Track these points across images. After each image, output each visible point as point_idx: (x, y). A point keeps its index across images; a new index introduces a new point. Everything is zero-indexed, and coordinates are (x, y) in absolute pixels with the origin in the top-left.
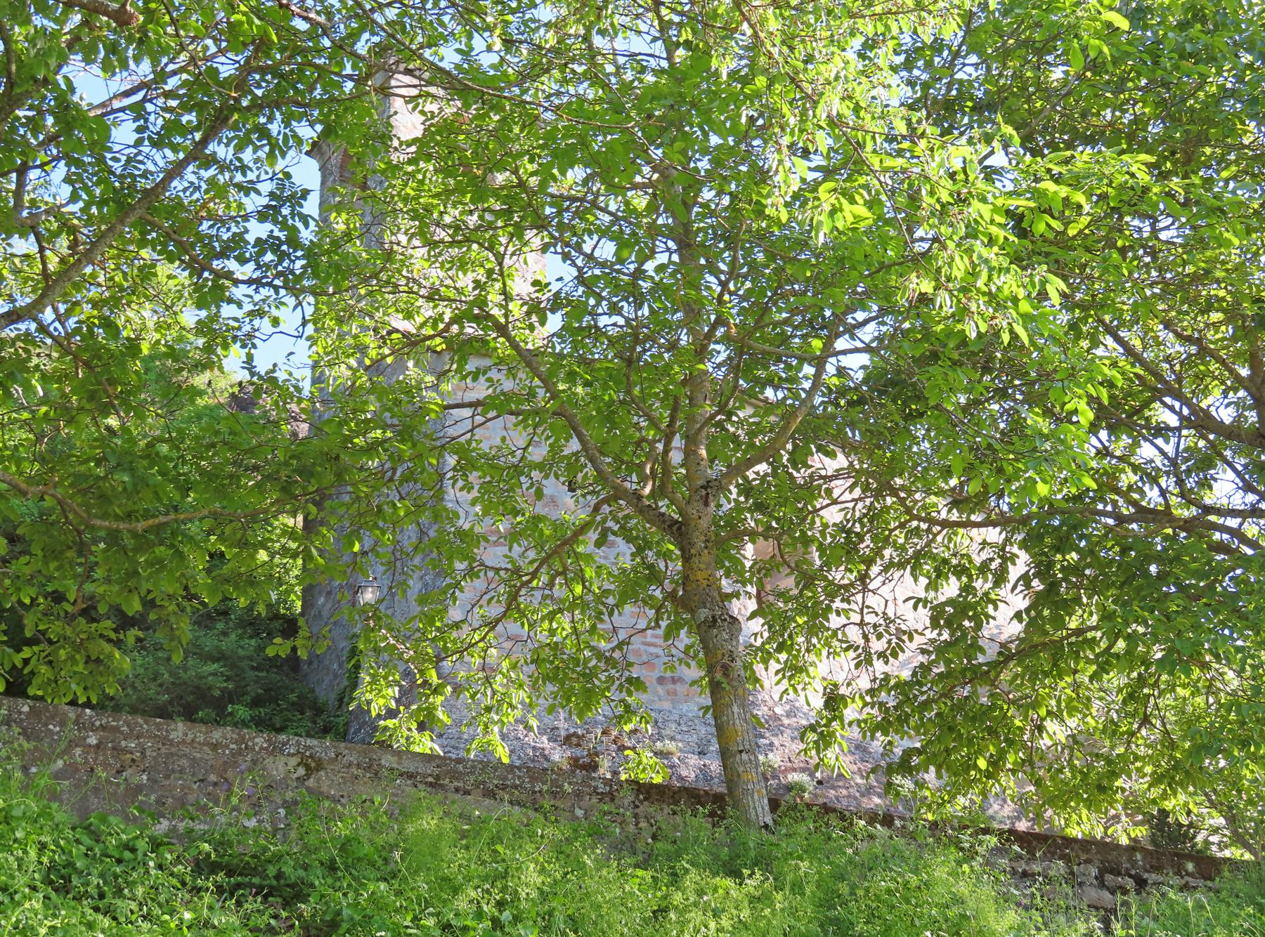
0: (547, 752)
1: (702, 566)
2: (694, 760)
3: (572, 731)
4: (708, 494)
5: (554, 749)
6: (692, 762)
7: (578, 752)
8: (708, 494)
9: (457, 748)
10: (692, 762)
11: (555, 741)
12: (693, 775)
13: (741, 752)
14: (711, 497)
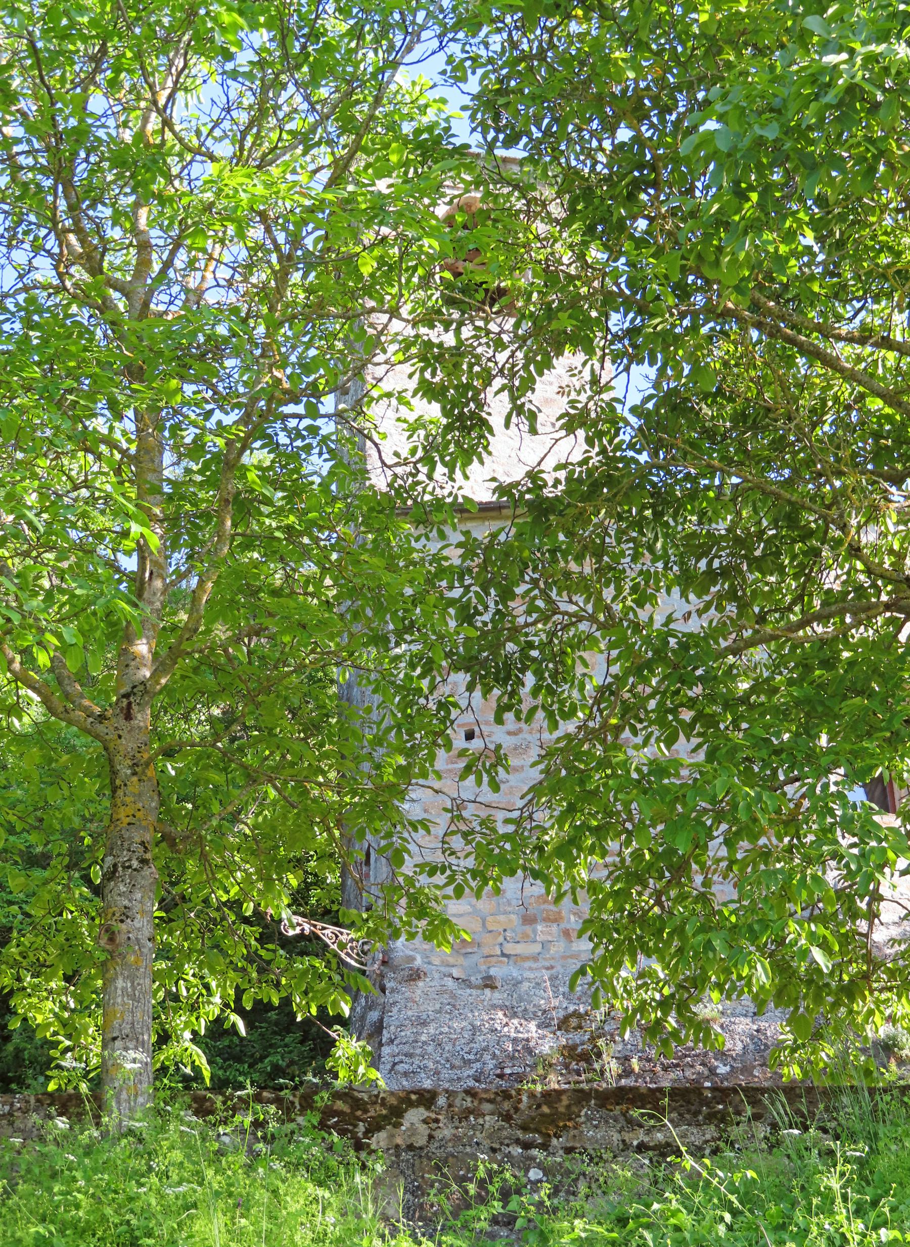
0: (532, 1044)
1: (128, 800)
2: (744, 1025)
3: (572, 1008)
4: (130, 704)
5: (543, 1037)
6: (739, 1028)
7: (576, 1037)
8: (130, 704)
9: (410, 1055)
10: (739, 1028)
11: (548, 1026)
12: (739, 1046)
13: (114, 1039)
14: (135, 708)
